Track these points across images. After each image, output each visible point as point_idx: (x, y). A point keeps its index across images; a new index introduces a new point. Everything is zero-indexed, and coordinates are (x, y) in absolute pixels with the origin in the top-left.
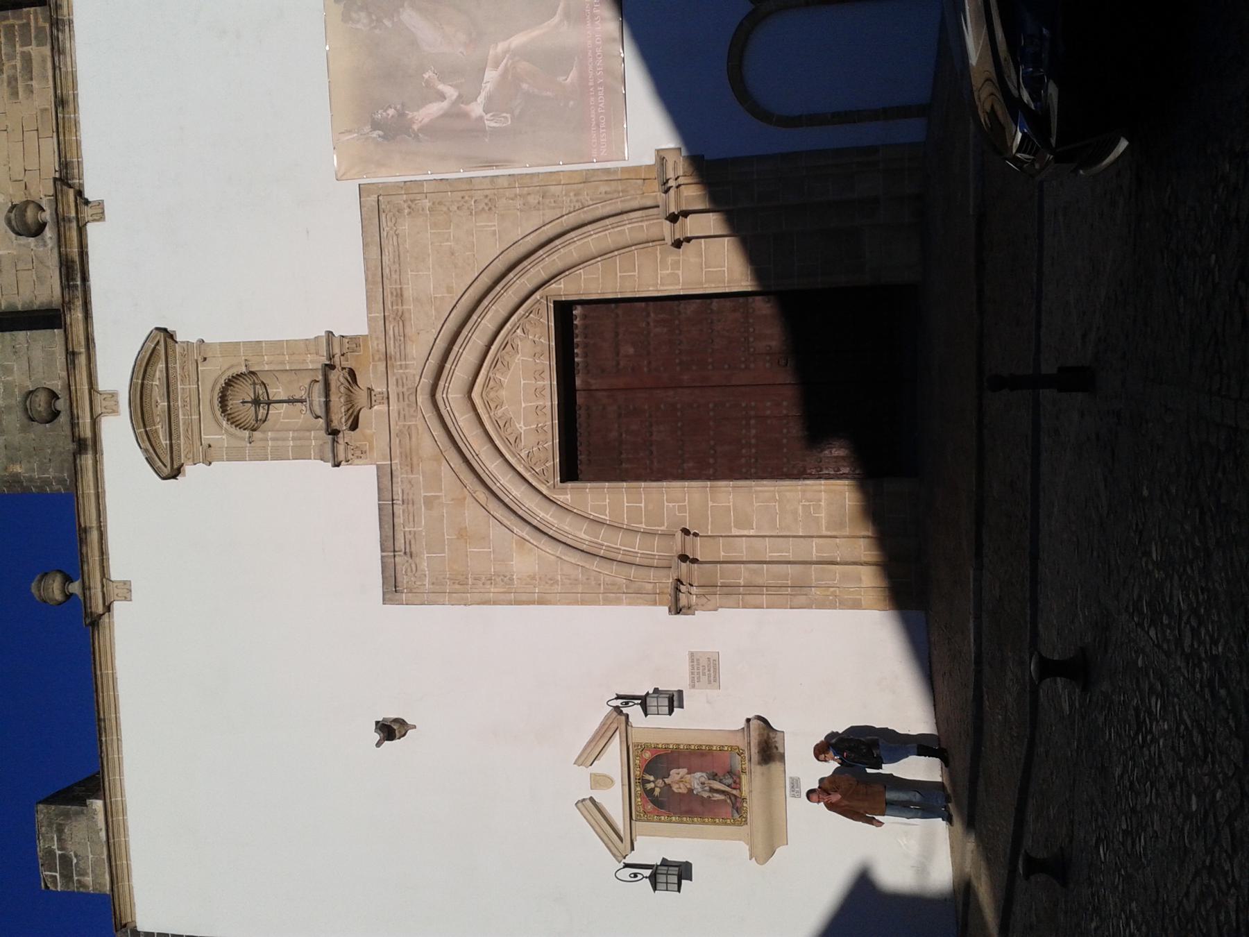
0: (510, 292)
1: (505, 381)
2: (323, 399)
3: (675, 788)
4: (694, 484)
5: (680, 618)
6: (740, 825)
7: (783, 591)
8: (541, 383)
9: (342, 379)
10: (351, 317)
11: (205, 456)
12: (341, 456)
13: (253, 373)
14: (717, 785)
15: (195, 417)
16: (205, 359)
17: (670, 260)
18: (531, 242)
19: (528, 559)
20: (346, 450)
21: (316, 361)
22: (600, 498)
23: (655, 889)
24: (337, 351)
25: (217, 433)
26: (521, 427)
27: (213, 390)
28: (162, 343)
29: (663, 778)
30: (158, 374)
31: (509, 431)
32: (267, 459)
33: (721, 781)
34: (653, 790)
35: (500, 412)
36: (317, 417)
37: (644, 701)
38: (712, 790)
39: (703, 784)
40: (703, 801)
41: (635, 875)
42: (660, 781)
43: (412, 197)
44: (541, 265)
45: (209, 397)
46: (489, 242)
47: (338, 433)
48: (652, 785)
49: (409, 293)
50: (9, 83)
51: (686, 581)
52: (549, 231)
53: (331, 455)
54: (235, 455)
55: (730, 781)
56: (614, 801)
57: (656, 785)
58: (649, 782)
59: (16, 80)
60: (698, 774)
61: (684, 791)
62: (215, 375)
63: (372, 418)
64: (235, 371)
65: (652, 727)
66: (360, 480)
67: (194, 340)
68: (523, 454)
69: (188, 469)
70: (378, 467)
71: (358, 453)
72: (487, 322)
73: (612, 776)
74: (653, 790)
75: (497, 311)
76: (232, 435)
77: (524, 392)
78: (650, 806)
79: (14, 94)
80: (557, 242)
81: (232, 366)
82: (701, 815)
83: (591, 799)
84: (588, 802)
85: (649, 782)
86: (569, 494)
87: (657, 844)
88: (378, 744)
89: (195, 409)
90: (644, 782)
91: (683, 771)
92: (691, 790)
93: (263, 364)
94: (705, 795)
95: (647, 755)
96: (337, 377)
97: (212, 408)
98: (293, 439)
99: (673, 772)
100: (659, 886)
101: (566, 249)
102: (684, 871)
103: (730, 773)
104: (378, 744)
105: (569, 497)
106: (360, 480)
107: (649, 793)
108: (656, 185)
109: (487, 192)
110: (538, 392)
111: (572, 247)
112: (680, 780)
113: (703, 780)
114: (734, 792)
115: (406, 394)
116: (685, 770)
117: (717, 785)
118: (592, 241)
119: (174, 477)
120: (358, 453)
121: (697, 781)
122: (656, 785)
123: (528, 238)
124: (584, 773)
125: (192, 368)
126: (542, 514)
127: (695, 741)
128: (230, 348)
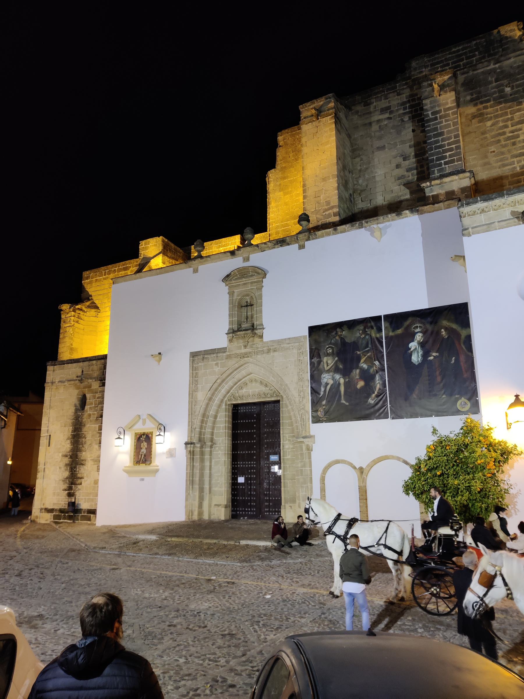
4: (281, 432)
7: (191, 477)
14: (143, 456)
19: (201, 396)
26: (244, 390)
38: (142, 455)
49: (276, 354)
50: (402, 176)
51: (197, 447)
59: (404, 178)
78: (138, 436)
79: (399, 179)
90: (144, 435)
95: (150, 436)
103: (146, 461)
112: (144, 445)
117: (143, 456)
121: (144, 451)
126: (217, 399)
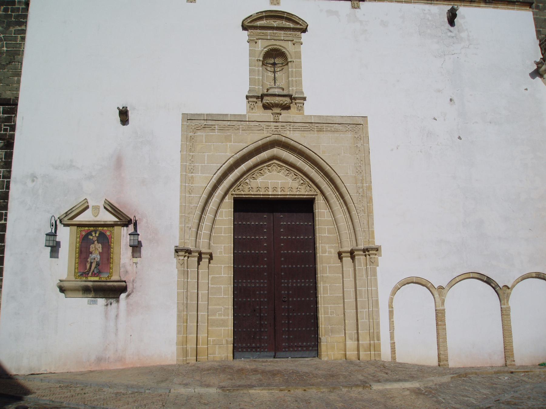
0: (321, 179)
1: (280, 174)
2: (277, 93)
3: (92, 246)
5: (174, 251)
6: (75, 275)
8: (279, 190)
9: (286, 102)
10: (312, 109)
11: (251, 40)
12: (250, 99)
13: (287, 64)
14: (94, 265)
15: (269, 37)
16: (294, 44)
17: (333, 250)
18: (343, 190)
20: (254, 102)
21: (292, 90)
22: (227, 214)
23: (47, 235)
24: (297, 101)
25: (261, 47)
27: (281, 46)
28: (301, 27)
29: (97, 240)
30: (288, 23)
31: (258, 175)
32: (250, 66)
33: (95, 267)
34: (92, 235)
35: (267, 171)
36: (268, 90)
37: (135, 234)
38: (91, 263)
39: (94, 259)
40: (87, 258)
41: (53, 226)
42: (96, 239)
43: (362, 139)
44: (332, 193)
45: (278, 44)
46: (343, 170)
47: (264, 100)
48: (94, 235)
49: (322, 134)
52: (347, 197)
53: (251, 95)
54: (252, 53)
55: (95, 272)
56: (86, 217)
57: (94, 236)
58: (96, 233)
60: (99, 257)
61: (91, 250)
62: (286, 47)
63: (268, 115)
64: (289, 56)
65: (123, 235)
66: (239, 106)
67: (302, 40)
68: (247, 181)
69: (246, 32)
70: (245, 115)
71: (252, 107)
72: (306, 167)
73: (99, 215)
74: (92, 235)
75: (312, 172)
76: (261, 52)
77: (274, 182)
80: (345, 208)
81: (291, 55)
82: (80, 257)
83: (87, 207)
84: (86, 205)
85: (96, 233)
86: (229, 201)
87: (65, 235)
88: (118, 108)
89: (272, 37)
91: (100, 250)
92: (91, 253)
93: (291, 68)
94: (89, 260)
95: (108, 233)
96: (287, 100)
97: (274, 45)
98: (259, 79)
99: (100, 245)
100: (48, 237)
101: (338, 205)
102: (55, 250)
104: (118, 108)
105: (227, 201)
106: (239, 106)
107: (90, 233)
108: (367, 246)
109: (364, 171)
110: (275, 189)
111: (339, 207)
112: (96, 249)
113: (96, 259)
114: (90, 274)
115: (278, 130)
116: (101, 251)
117: (94, 265)
118: (341, 215)
119: (242, 26)
120: (252, 107)
121: (95, 256)
122: (94, 236)
123: (345, 188)
124: (101, 204)
125: (290, 38)
127: (115, 256)
128: (298, 55)
